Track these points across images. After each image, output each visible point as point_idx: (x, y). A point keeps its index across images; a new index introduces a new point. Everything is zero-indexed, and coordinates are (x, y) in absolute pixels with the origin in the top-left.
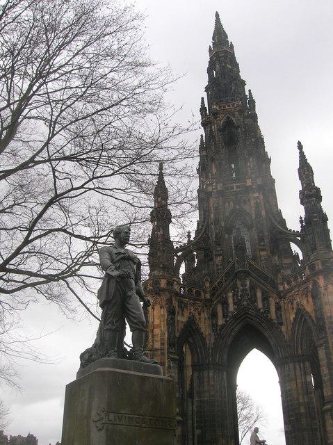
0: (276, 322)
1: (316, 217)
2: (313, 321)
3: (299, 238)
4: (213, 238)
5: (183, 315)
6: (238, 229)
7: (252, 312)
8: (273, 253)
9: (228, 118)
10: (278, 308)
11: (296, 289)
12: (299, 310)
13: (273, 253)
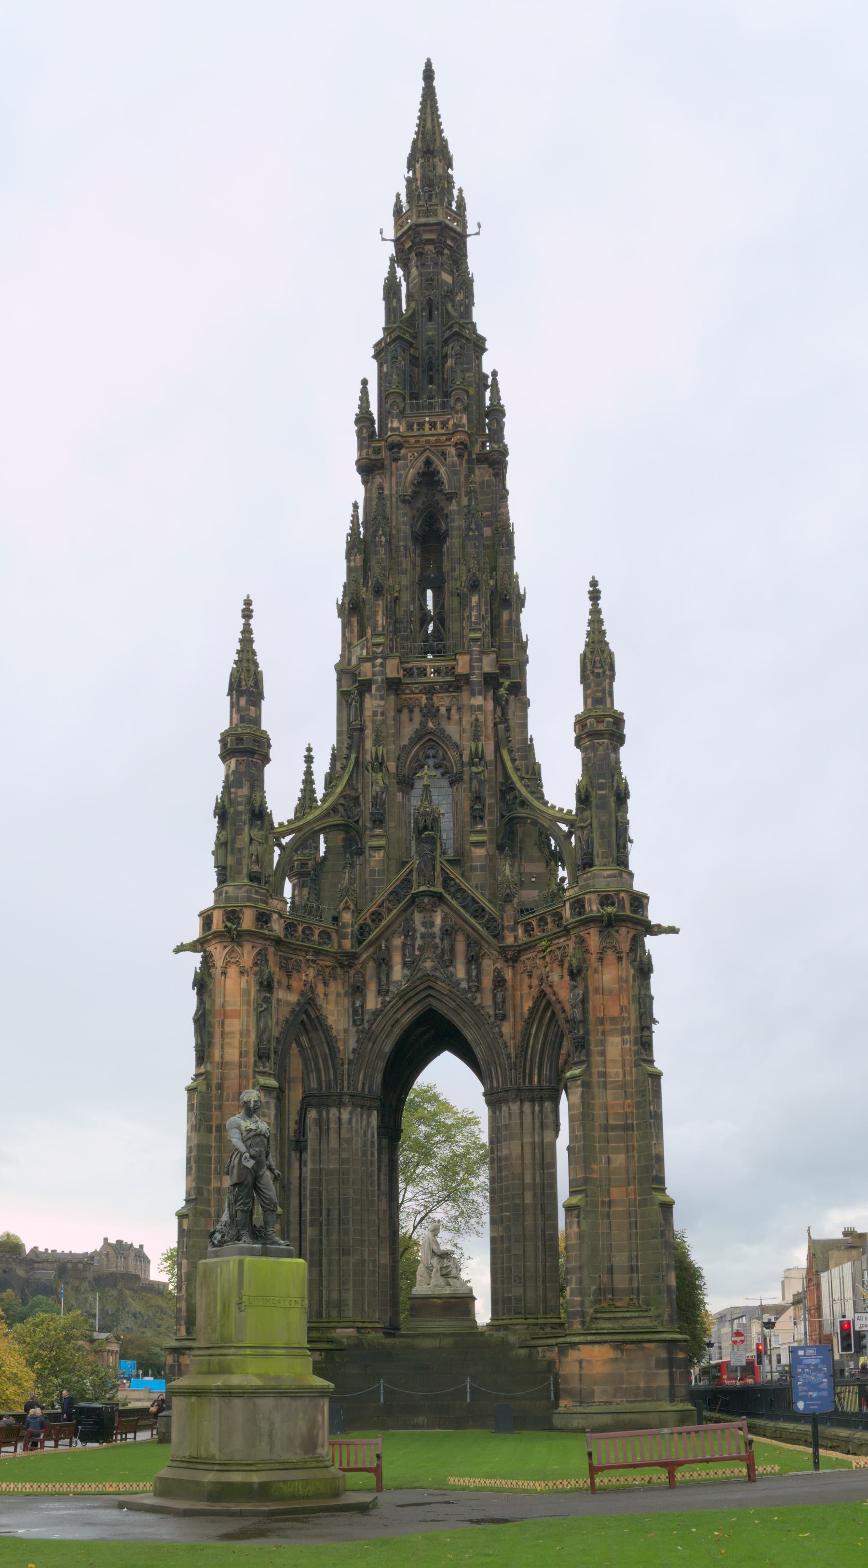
4: (367, 807)
7: (441, 985)
9: (428, 463)
10: (499, 982)
12: (543, 994)
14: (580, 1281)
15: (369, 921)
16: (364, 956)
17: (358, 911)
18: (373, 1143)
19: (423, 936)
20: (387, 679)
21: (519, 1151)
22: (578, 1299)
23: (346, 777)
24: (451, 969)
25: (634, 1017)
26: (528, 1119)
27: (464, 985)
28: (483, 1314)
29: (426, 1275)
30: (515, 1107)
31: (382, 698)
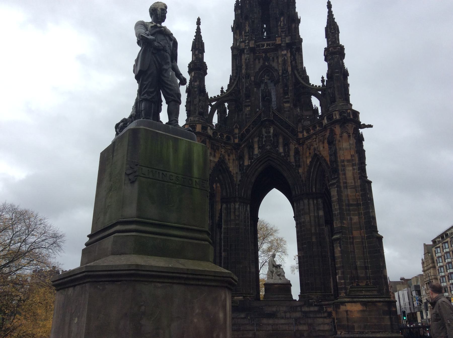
0: (294, 164)
1: (337, 72)
2: (327, 164)
3: (320, 92)
5: (215, 156)
6: (266, 83)
8: (295, 106)
10: (297, 152)
11: (314, 137)
13: (295, 106)
14: (343, 273)
15: (245, 132)
16: (243, 146)
17: (240, 129)
18: (248, 217)
19: (266, 137)
20: (250, 48)
21: (309, 219)
22: (343, 281)
23: (235, 83)
24: (277, 149)
25: (357, 159)
26: (312, 206)
27: (283, 154)
28: (296, 292)
29: (271, 275)
30: (306, 201)
31: (248, 54)
